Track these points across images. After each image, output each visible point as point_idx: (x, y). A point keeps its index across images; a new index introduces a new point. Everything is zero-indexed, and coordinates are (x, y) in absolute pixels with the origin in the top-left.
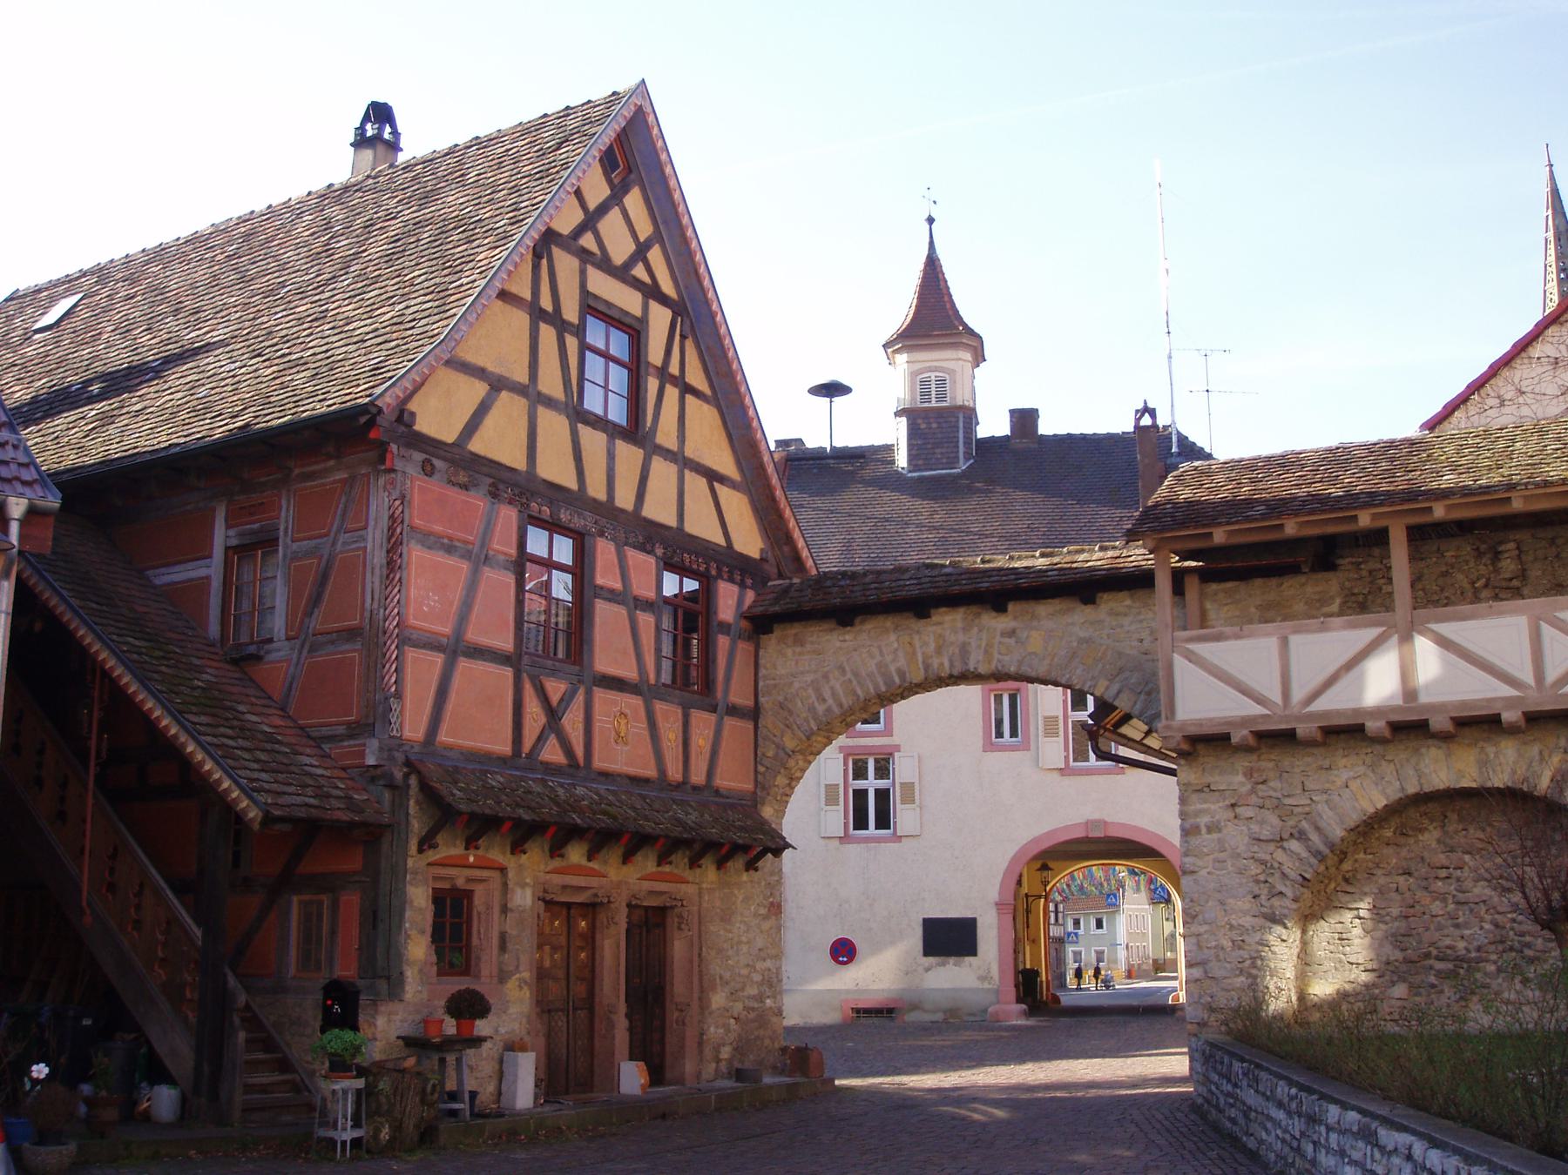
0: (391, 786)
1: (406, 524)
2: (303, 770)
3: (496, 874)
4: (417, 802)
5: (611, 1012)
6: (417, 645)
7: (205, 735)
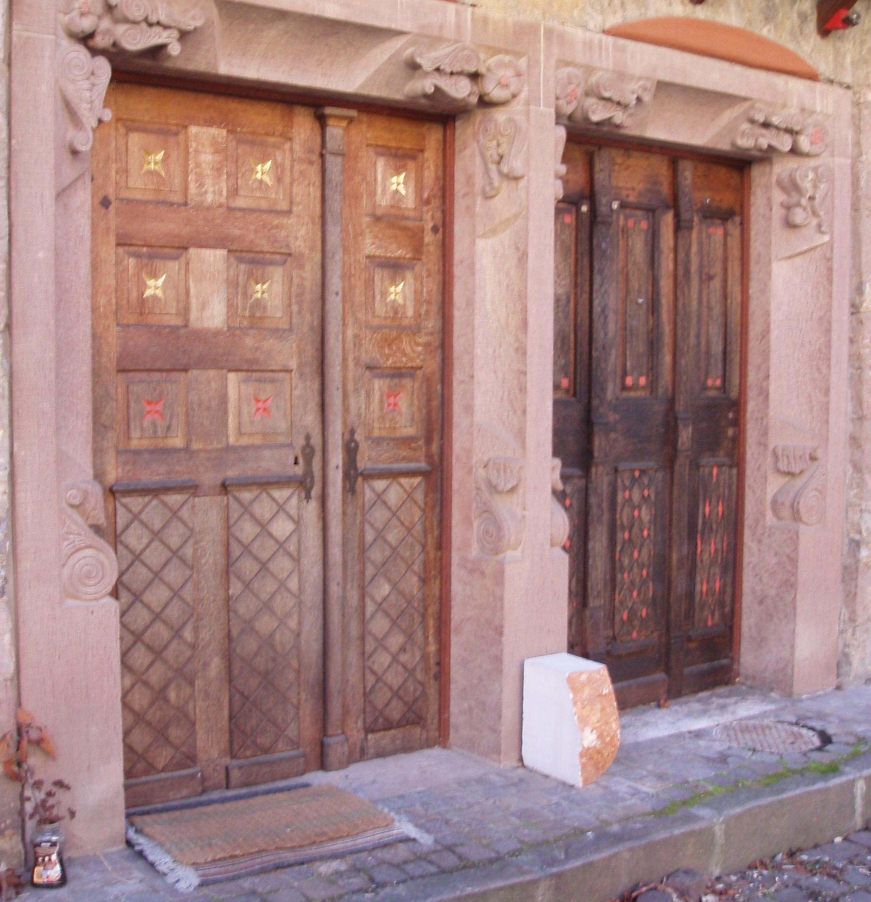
5: (493, 488)
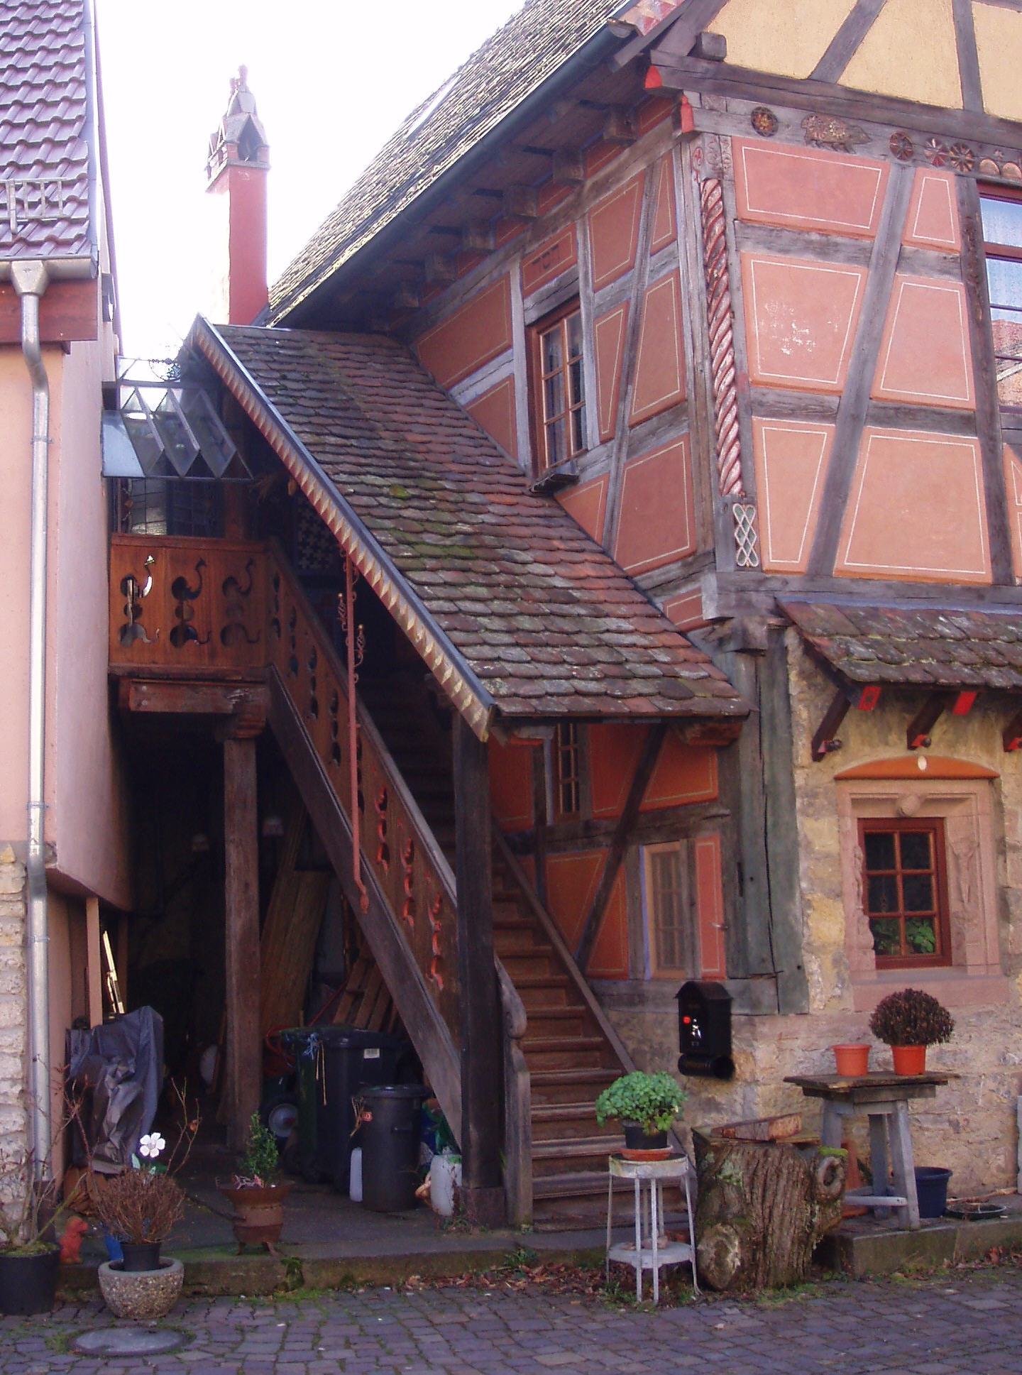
0: (748, 651)
1: (731, 215)
2: (599, 639)
3: (980, 788)
4: (802, 674)
6: (775, 412)
7: (430, 599)
